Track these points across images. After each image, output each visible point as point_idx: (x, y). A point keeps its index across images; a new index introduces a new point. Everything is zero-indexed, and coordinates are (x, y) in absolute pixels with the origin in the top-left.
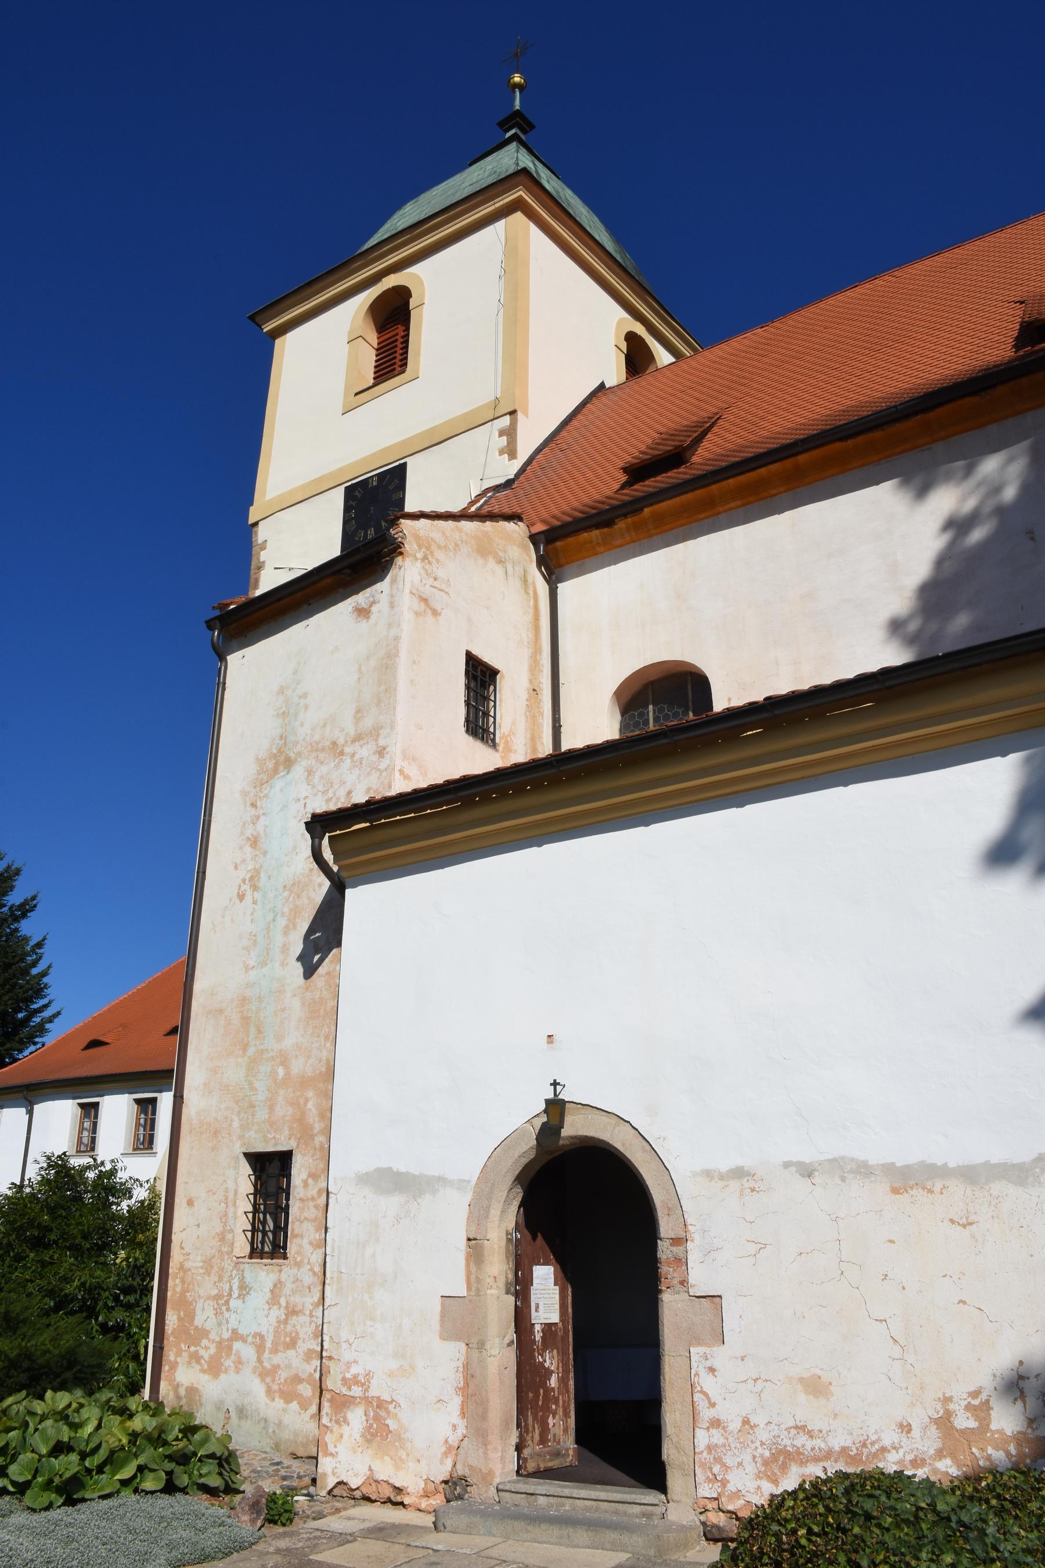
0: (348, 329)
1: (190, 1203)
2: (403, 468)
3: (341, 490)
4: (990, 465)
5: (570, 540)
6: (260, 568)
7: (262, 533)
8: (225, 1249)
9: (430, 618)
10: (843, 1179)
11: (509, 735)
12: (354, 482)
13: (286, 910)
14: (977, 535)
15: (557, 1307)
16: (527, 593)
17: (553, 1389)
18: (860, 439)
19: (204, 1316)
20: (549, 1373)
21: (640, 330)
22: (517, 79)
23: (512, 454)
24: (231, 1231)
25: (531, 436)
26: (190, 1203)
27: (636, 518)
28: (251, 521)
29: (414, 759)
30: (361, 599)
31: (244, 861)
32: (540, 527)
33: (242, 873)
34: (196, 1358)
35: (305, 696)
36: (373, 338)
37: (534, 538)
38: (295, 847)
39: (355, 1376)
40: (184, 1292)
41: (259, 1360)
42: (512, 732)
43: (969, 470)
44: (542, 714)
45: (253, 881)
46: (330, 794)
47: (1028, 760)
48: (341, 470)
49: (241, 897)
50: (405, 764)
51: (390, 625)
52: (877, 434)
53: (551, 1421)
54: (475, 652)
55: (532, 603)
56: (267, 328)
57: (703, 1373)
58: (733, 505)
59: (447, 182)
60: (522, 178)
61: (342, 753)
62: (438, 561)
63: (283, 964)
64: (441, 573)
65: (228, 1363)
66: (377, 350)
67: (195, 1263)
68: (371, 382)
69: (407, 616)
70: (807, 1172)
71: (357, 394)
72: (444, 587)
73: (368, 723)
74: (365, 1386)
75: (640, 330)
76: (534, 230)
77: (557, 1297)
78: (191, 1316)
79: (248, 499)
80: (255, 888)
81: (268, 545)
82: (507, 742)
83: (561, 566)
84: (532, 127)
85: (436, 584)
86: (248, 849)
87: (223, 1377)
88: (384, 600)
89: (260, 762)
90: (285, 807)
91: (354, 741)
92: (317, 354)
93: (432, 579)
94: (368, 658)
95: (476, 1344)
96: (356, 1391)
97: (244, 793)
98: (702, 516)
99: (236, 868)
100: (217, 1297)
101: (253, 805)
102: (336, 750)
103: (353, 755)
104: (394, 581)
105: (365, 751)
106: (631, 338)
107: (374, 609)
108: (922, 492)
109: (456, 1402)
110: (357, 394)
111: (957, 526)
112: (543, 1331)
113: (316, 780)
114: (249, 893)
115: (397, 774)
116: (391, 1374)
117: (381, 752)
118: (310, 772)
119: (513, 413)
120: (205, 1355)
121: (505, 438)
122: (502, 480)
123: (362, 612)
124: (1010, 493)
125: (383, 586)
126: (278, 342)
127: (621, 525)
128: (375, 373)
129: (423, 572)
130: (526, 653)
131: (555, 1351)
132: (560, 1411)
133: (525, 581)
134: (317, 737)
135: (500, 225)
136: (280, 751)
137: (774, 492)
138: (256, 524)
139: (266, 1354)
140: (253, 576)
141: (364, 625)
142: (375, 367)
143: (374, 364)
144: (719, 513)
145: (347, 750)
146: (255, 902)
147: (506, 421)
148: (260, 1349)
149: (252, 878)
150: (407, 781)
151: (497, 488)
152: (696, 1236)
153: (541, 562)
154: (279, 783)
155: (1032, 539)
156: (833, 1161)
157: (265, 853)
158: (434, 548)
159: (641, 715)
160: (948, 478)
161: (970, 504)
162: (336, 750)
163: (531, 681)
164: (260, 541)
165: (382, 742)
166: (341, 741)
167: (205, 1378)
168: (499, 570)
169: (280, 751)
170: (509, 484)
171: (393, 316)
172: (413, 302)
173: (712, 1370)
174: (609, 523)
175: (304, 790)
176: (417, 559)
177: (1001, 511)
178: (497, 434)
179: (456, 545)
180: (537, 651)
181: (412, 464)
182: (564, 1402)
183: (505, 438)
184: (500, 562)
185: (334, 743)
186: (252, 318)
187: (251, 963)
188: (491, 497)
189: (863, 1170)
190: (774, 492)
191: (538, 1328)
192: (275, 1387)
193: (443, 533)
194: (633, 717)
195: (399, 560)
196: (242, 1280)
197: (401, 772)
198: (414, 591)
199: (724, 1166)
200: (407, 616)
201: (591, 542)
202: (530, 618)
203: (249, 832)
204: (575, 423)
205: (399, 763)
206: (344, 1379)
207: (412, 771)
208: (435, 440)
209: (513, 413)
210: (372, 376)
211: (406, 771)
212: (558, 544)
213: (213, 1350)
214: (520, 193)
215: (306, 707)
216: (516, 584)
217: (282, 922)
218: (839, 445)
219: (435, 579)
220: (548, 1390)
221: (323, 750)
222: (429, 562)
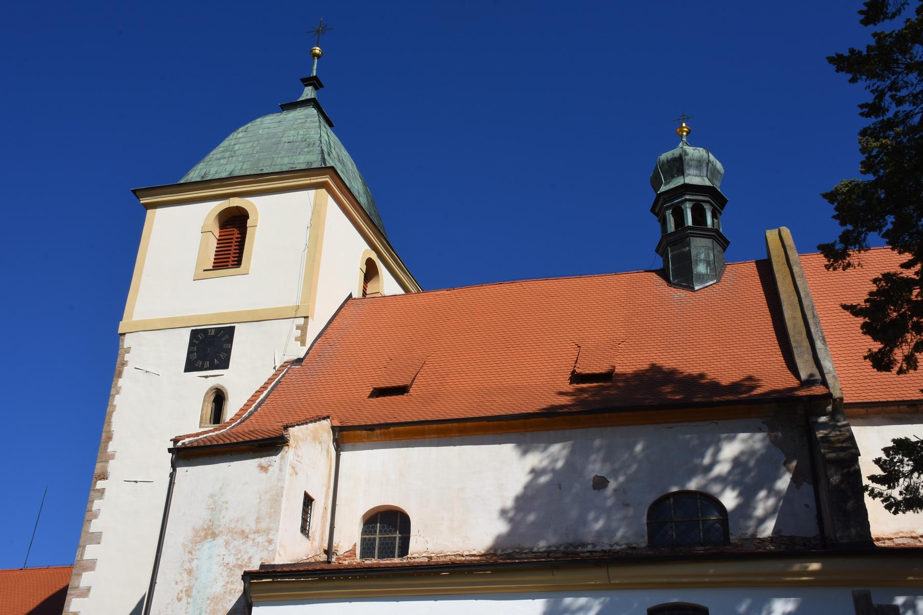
4: (555, 448)
7: (128, 341)
13: (208, 610)
14: (543, 479)
22: (317, 50)
23: (303, 343)
27: (386, 431)
28: (120, 331)
30: (264, 461)
31: (182, 581)
33: (180, 587)
35: (226, 502)
36: (217, 232)
37: (333, 428)
38: (215, 579)
43: (545, 449)
45: (188, 592)
46: (239, 556)
49: (179, 600)
51: (279, 480)
60: (330, 171)
61: (247, 537)
64: (300, 453)
69: (287, 476)
73: (263, 525)
76: (330, 200)
80: (189, 596)
84: (322, 86)
86: (185, 575)
88: (276, 466)
89: (196, 531)
90: (210, 557)
91: (254, 533)
92: (175, 234)
94: (266, 493)
97: (184, 545)
99: (177, 583)
101: (190, 552)
102: (244, 535)
103: (254, 540)
104: (282, 458)
105: (261, 539)
106: (370, 263)
107: (270, 468)
108: (525, 452)
111: (535, 472)
113: (231, 547)
114: (185, 598)
118: (227, 543)
123: (264, 469)
124: (560, 464)
125: (276, 459)
127: (378, 431)
130: (325, 489)
134: (232, 526)
135: (312, 193)
136: (209, 527)
138: (124, 334)
141: (263, 475)
145: (250, 536)
146: (188, 603)
147: (301, 321)
149: (187, 591)
153: (335, 440)
154: (207, 544)
157: (196, 579)
159: (373, 527)
160: (536, 449)
161: (545, 463)
162: (244, 535)
165: (271, 537)
166: (247, 531)
170: (299, 361)
171: (234, 224)
172: (249, 222)
175: (223, 551)
177: (553, 470)
178: (295, 327)
180: (329, 488)
184: (320, 443)
185: (243, 531)
186: (134, 192)
194: (368, 528)
195: (286, 448)
200: (287, 476)
203: (187, 566)
204: (334, 322)
205: (278, 548)
209: (306, 317)
214: (326, 179)
215: (227, 509)
216: (325, 453)
218: (486, 423)
221: (236, 533)
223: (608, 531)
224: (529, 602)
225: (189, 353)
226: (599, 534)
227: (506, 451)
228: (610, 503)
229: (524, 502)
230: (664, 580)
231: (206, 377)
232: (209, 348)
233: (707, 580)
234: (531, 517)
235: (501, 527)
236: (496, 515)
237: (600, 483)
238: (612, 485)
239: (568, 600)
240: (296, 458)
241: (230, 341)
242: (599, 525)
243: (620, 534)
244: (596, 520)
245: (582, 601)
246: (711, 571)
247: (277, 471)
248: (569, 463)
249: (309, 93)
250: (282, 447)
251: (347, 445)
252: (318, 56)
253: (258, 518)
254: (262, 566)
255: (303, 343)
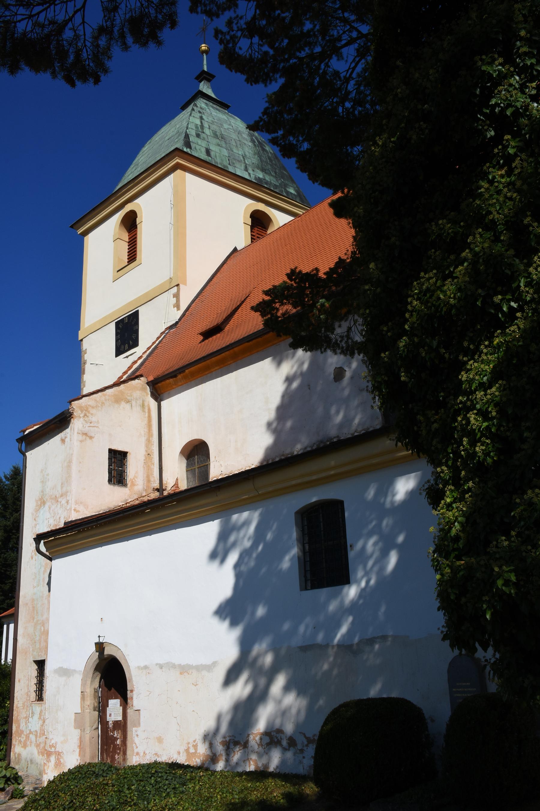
0: (113, 234)
1: (19, 681)
2: (137, 313)
3: (114, 323)
5: (163, 383)
6: (85, 363)
7: (85, 345)
8: (28, 699)
9: (88, 441)
10: (169, 670)
11: (134, 479)
12: (119, 319)
14: (295, 385)
15: (121, 714)
16: (144, 411)
17: (118, 745)
18: (254, 341)
19: (23, 726)
20: (116, 739)
21: (261, 207)
23: (178, 309)
24: (30, 691)
25: (188, 296)
26: (19, 681)
27: (184, 374)
28: (80, 339)
29: (81, 503)
32: (151, 378)
34: (20, 742)
39: (53, 744)
40: (18, 716)
41: (36, 741)
42: (136, 477)
43: (294, 355)
44: (153, 464)
47: (221, 521)
48: (113, 313)
49: (32, 558)
50: (77, 506)
52: (259, 339)
53: (116, 756)
54: (114, 448)
55: (147, 415)
56: (80, 231)
57: (135, 736)
58: (216, 368)
59: (178, 116)
62: (92, 414)
63: (43, 586)
64: (94, 419)
65: (28, 743)
66: (129, 242)
67: (20, 705)
68: (127, 264)
70: (161, 667)
71: (118, 271)
72: (95, 425)
74: (55, 747)
75: (261, 207)
77: (121, 711)
78: (19, 726)
79: (78, 327)
81: (88, 351)
82: (132, 482)
83: (162, 393)
84: (213, 77)
85: (92, 425)
87: (27, 748)
93: (89, 424)
95: (83, 730)
96: (53, 750)
98: (206, 373)
100: (26, 717)
108: (279, 364)
109: (78, 751)
110: (118, 271)
111: (289, 380)
112: (113, 723)
115: (73, 511)
116: (62, 743)
117: (67, 502)
118: (50, 508)
119: (178, 285)
120: (22, 740)
121: (175, 299)
122: (174, 322)
124: (306, 366)
125: (68, 430)
126: (85, 238)
127: (179, 377)
128: (128, 256)
129: (84, 422)
130: (143, 439)
131: (120, 731)
132: (122, 753)
133: (143, 406)
134: (51, 493)
137: (229, 363)
138: (82, 340)
139: (38, 738)
140: (82, 368)
142: (128, 252)
143: (127, 251)
144: (212, 372)
147: (175, 290)
148: (36, 736)
150: (78, 513)
151: (171, 327)
152: (135, 689)
154: (42, 511)
155: (309, 388)
156: (167, 663)
158: (90, 409)
160: (287, 357)
163: (146, 451)
164: (84, 349)
166: (58, 496)
167: (23, 749)
168: (128, 406)
169: (42, 498)
172: (138, 221)
173: (137, 735)
174: (175, 376)
176: (80, 417)
177: (302, 374)
179: (103, 403)
181: (142, 311)
182: (123, 749)
183: (175, 299)
184: (128, 402)
185: (56, 496)
187: (35, 585)
188: (167, 333)
189: (174, 666)
190: (229, 363)
191: (110, 722)
192: (40, 751)
193: (95, 400)
196: (32, 711)
197: (75, 510)
198: (80, 432)
199: (142, 665)
201: (170, 384)
202: (146, 422)
206: (50, 745)
207: (81, 508)
208: (149, 298)
210: (127, 257)
211: (77, 509)
212: (159, 385)
213: (24, 739)
216: (137, 409)
217: (43, 569)
218: (247, 344)
219: (91, 423)
220: (115, 746)
222: (87, 417)
223: (347, 421)
224: (211, 523)
225: (117, 341)
226: (341, 426)
227: (266, 365)
228: (346, 392)
229: (283, 411)
230: (299, 481)
231: (127, 357)
232: (127, 332)
233: (332, 472)
234: (289, 424)
235: (266, 440)
236: (264, 428)
237: (339, 374)
238: (348, 374)
239: (235, 517)
240: (89, 424)
241: (137, 323)
242: (339, 418)
243: (357, 421)
244: (338, 412)
245: (245, 514)
246: (333, 463)
247: (69, 441)
248: (313, 363)
249: (205, 87)
250: (70, 420)
251: (165, 395)
252: (206, 52)
253: (62, 484)
254: (65, 523)
255: (178, 309)
